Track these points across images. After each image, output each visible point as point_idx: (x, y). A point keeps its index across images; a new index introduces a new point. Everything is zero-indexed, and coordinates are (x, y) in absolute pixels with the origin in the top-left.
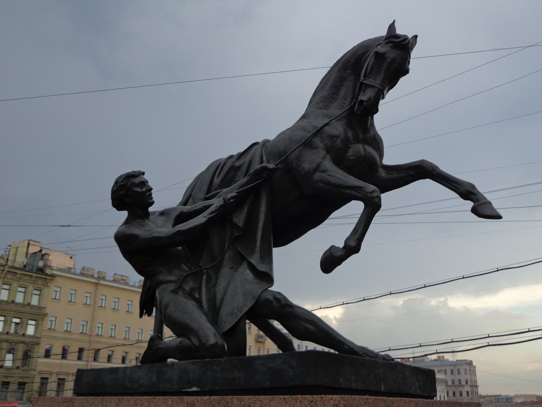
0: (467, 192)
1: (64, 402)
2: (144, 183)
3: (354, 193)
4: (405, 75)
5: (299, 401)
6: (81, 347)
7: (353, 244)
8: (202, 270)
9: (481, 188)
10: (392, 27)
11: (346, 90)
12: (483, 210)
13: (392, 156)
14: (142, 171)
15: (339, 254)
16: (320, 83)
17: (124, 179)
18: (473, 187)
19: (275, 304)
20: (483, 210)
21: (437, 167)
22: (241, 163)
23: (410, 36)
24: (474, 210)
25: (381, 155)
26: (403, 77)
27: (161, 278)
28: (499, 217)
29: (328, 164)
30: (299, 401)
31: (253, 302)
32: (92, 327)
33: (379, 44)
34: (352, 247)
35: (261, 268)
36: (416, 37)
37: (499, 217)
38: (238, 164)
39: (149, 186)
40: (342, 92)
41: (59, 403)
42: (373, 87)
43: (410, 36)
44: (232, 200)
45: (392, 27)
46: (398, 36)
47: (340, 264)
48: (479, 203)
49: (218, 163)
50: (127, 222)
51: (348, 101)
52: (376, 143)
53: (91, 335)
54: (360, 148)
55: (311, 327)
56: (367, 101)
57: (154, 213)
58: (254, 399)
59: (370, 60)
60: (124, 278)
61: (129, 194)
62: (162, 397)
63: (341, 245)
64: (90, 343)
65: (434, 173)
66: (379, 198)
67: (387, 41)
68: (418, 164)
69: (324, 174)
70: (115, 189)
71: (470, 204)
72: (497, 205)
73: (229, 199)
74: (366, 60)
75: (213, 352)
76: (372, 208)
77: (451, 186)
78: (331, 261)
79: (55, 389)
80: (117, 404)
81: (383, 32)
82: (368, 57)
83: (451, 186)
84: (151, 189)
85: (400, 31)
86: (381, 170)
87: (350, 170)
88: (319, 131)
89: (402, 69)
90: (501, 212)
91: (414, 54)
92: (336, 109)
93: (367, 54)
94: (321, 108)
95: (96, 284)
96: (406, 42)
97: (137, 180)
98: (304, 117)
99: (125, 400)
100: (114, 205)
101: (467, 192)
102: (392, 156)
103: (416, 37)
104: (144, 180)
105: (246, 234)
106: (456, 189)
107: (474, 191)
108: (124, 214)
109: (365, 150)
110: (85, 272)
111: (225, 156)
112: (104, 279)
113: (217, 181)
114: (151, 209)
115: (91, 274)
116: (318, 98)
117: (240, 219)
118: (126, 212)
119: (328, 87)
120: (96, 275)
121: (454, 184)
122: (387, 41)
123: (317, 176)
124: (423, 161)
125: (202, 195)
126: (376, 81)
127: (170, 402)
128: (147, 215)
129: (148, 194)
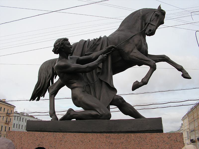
0: (180, 69)
3: (145, 62)
5: (164, 135)
7: (145, 81)
10: (160, 7)
12: (186, 76)
19: (120, 100)
20: (186, 76)
22: (99, 43)
24: (182, 75)
29: (136, 50)
30: (164, 135)
31: (112, 99)
34: (145, 82)
38: (98, 43)
44: (106, 57)
45: (160, 7)
56: (153, 30)
58: (91, 137)
61: (64, 47)
65: (169, 60)
71: (181, 73)
76: (153, 68)
77: (174, 66)
78: (136, 86)
83: (175, 66)
84: (62, 47)
98: (118, 30)
99: (68, 134)
101: (180, 69)
103: (33, 98)
104: (92, 42)
105: (103, 72)
106: (176, 67)
118: (59, 54)
122: (159, 11)
123: (132, 54)
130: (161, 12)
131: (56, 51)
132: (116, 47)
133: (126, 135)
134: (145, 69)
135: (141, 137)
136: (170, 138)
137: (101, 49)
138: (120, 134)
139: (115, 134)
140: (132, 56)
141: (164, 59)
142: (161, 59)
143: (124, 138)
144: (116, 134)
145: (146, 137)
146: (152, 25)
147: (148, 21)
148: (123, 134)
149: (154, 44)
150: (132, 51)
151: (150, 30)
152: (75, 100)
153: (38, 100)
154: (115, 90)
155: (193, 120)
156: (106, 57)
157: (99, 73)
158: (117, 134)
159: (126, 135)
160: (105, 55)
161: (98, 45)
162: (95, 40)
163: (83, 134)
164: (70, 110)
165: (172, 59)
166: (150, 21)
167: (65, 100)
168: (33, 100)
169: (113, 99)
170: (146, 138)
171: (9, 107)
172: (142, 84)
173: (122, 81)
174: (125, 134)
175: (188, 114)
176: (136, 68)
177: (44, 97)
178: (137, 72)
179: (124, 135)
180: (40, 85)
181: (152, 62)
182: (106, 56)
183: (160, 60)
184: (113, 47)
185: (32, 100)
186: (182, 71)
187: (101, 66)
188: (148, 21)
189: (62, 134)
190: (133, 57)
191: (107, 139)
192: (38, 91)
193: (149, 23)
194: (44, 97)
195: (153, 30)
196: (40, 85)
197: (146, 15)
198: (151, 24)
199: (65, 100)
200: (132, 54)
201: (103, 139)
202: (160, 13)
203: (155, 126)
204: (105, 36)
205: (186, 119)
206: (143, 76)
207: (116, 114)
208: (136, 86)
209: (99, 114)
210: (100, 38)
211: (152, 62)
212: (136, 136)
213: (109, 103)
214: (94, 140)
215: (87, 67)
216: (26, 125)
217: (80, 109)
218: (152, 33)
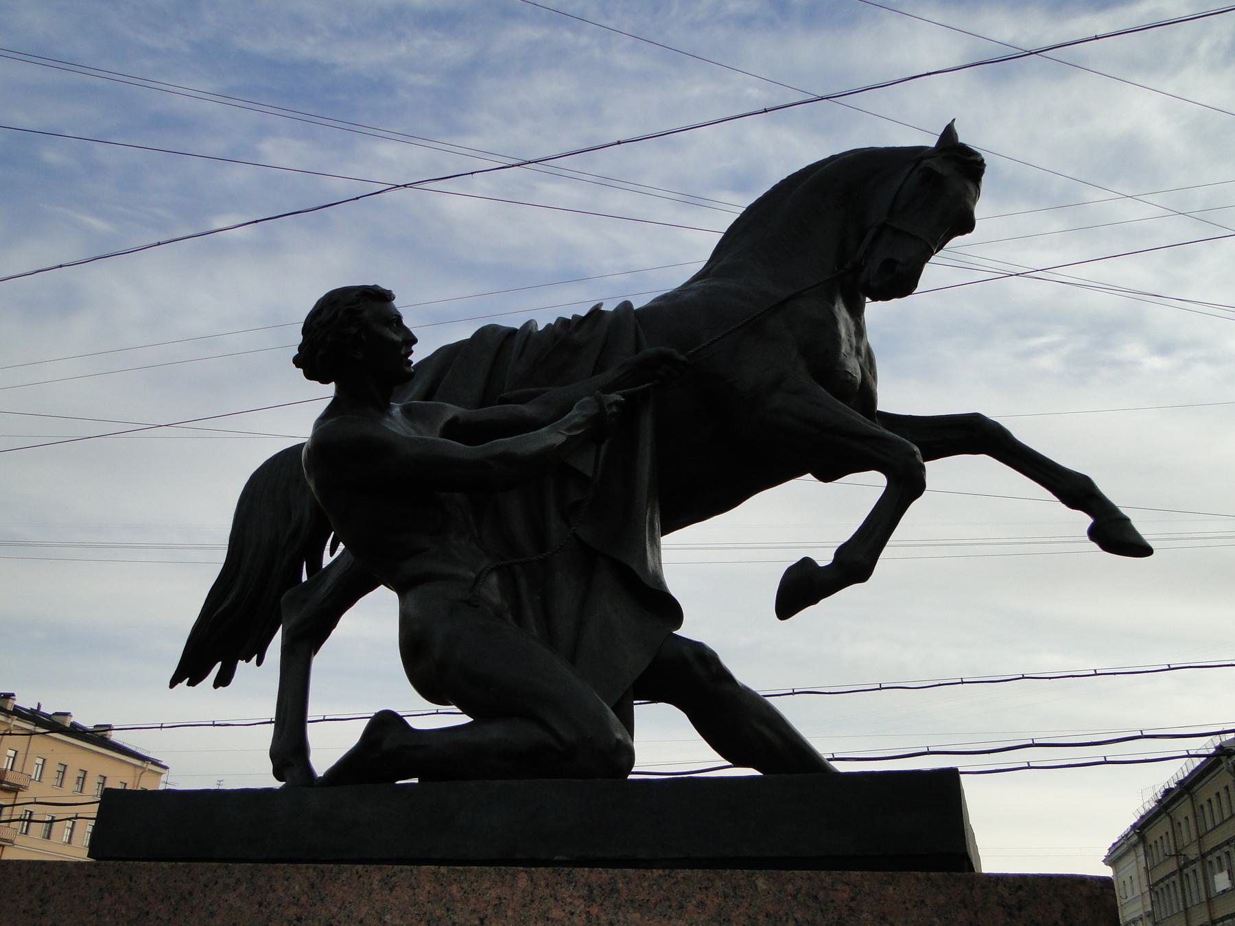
0: (1074, 490)
12: (1115, 535)
13: (897, 395)
20: (1115, 535)
24: (1095, 534)
34: (857, 560)
39: (407, 331)
72: (1144, 527)
76: (905, 488)
78: (801, 588)
84: (415, 341)
85: (962, 138)
99: (344, 876)
101: (1074, 490)
102: (897, 395)
103: (190, 669)
118: (332, 385)
131: (314, 358)
132: (683, 358)
133: (718, 883)
134: (865, 489)
135: (821, 895)
136: (1020, 909)
138: (681, 873)
139: (648, 874)
141: (975, 435)
143: (708, 902)
144: (657, 872)
145: (853, 899)
147: (889, 210)
148: (699, 872)
149: (919, 349)
151: (889, 265)
152: (425, 664)
153: (223, 680)
154: (672, 612)
155: (1172, 866)
156: (614, 409)
158: (661, 872)
159: (718, 883)
160: (616, 397)
162: (563, 322)
163: (443, 869)
164: (385, 725)
165: (1023, 434)
167: (364, 669)
168: (192, 683)
170: (852, 904)
171: (131, 769)
173: (718, 570)
174: (710, 873)
175: (1142, 827)
176: (803, 488)
177: (259, 663)
178: (809, 513)
179: (705, 884)
181: (905, 453)
185: (189, 684)
187: (586, 464)
189: (310, 871)
191: (595, 910)
194: (259, 663)
199: (364, 669)
201: (568, 908)
203: (921, 811)
204: (627, 305)
205: (1131, 858)
206: (847, 527)
207: (665, 743)
208: (801, 588)
210: (596, 312)
211: (905, 453)
212: (790, 888)
214: (510, 913)
217: (451, 718)
218: (900, 283)
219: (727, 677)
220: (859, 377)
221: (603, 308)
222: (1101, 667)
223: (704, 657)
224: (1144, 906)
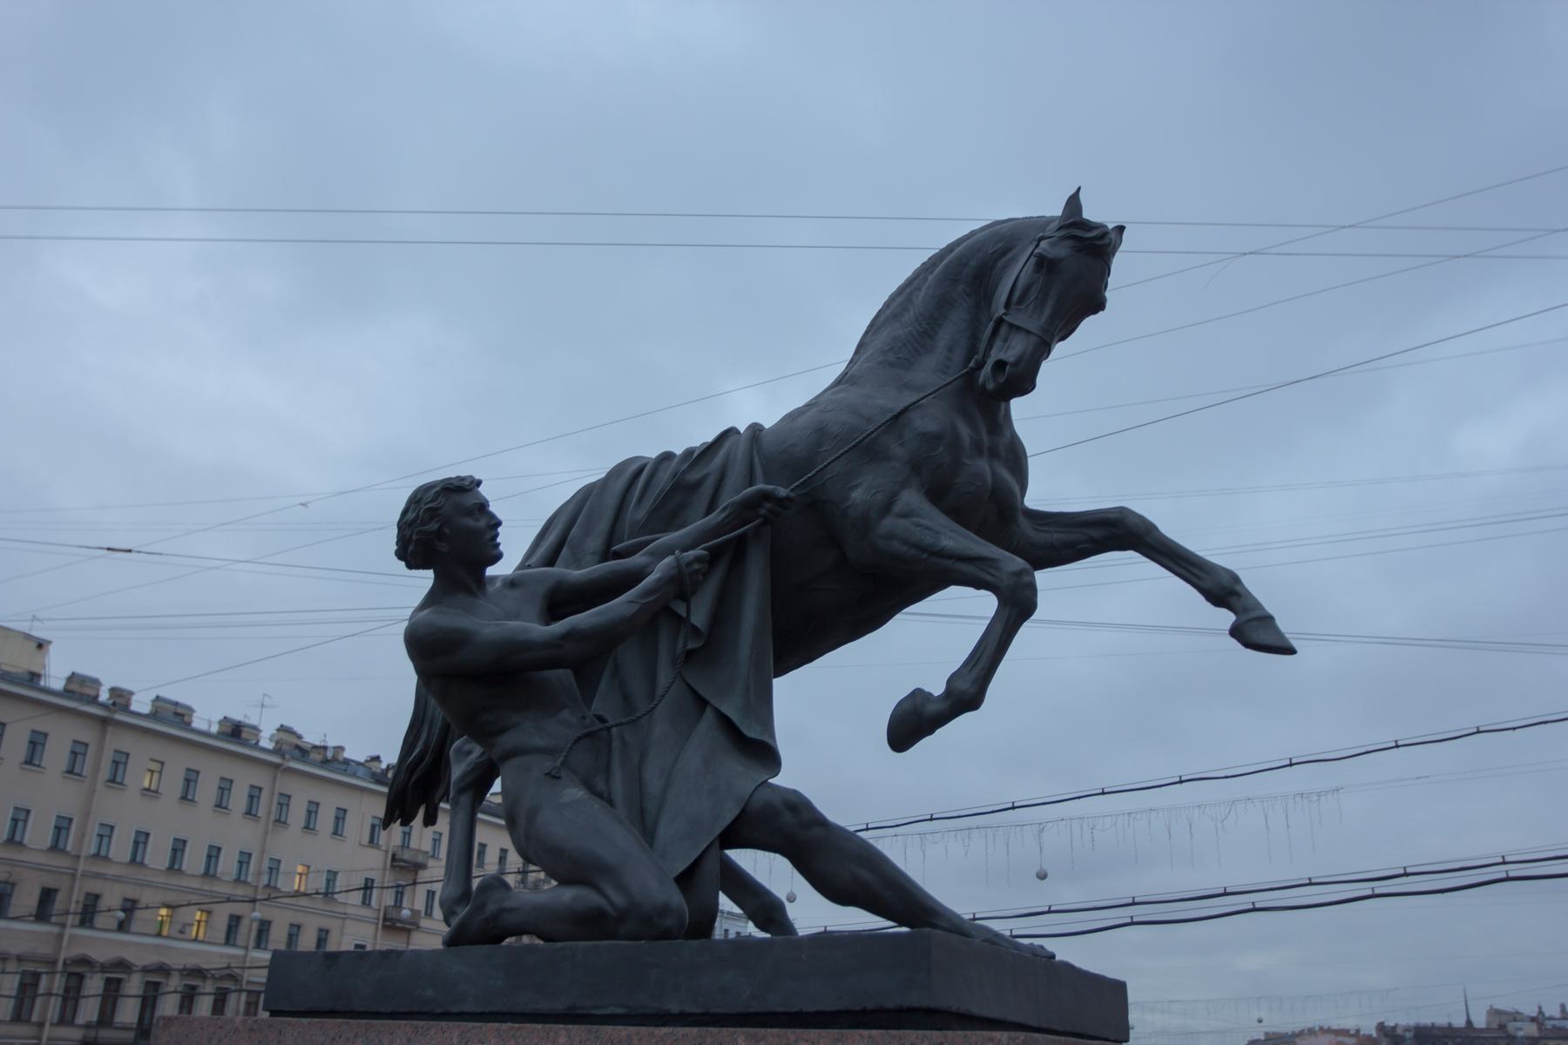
0: (1220, 588)
1: (251, 1030)
2: (483, 507)
4: (1095, 312)
6: (48, 885)
7: (964, 686)
8: (608, 729)
9: (1253, 583)
10: (1074, 203)
11: (951, 330)
12: (1258, 633)
13: (1049, 489)
14: (477, 477)
15: (932, 708)
16: (887, 305)
17: (438, 494)
18: (1236, 579)
19: (788, 818)
20: (1258, 633)
21: (1155, 528)
23: (1111, 226)
24: (1236, 632)
25: (1024, 487)
26: (1092, 317)
27: (507, 740)
28: (1290, 651)
29: (912, 498)
31: (737, 812)
32: (84, 835)
33: (1042, 238)
34: (966, 694)
35: (752, 732)
36: (1121, 229)
37: (1290, 651)
38: (694, 476)
39: (492, 516)
40: (945, 336)
41: (236, 1030)
42: (1029, 332)
43: (1111, 226)
44: (696, 566)
45: (1074, 203)
46: (1087, 226)
47: (930, 731)
48: (1252, 615)
49: (634, 467)
50: (431, 599)
51: (959, 355)
52: (1016, 460)
53: (78, 857)
54: (983, 465)
55: (865, 875)
56: (1015, 364)
57: (494, 578)
59: (1018, 270)
60: (179, 710)
61: (447, 531)
62: (539, 1026)
63: (937, 688)
64: (73, 876)
66: (1032, 588)
67: (1063, 233)
68: (1112, 516)
69: (903, 522)
70: (411, 516)
71: (1227, 618)
72: (1286, 625)
73: (689, 564)
74: (1006, 267)
75: (648, 926)
76: (1017, 607)
78: (912, 724)
79: (14, 993)
80: (409, 1040)
81: (1055, 209)
82: (1014, 260)
84: (499, 524)
85: (1090, 213)
86: (1022, 520)
87: (958, 515)
88: (898, 418)
89: (1087, 299)
90: (1295, 644)
91: (1119, 263)
92: (930, 372)
93: (1009, 255)
94: (892, 365)
95: (104, 722)
96: (1105, 241)
97: (468, 500)
98: (839, 382)
99: (432, 1032)
100: (402, 554)
101: (1220, 588)
102: (1049, 489)
103: (1121, 229)
105: (708, 650)
107: (1238, 588)
108: (425, 579)
109: (994, 473)
110: (74, 687)
111: (652, 453)
112: (125, 708)
113: (637, 513)
114: (491, 571)
115: (93, 693)
116: (885, 335)
117: (699, 615)
118: (430, 574)
119: (909, 316)
120: (104, 696)
121: (1196, 571)
122: (1063, 233)
124: (1122, 511)
125: (595, 543)
126: (1029, 319)
127: (562, 1040)
128: (480, 581)
129: (488, 536)
130: (1074, 237)
137: (708, 513)
140: (889, 537)
141: (1115, 532)
142: (1096, 533)
146: (1018, 328)
147: (1024, 288)
149: (1070, 434)
150: (886, 508)
154: (766, 755)
157: (690, 654)
161: (697, 485)
166: (1008, 305)
169: (743, 811)
172: (942, 706)
178: (934, 633)
180: (424, 736)
182: (698, 559)
183: (1092, 540)
184: (765, 496)
186: (1234, 600)
188: (1024, 288)
190: (896, 546)
192: (412, 772)
193: (1000, 321)
195: (1020, 359)
196: (424, 736)
197: (1000, 263)
198: (1011, 326)
200: (888, 523)
202: (1070, 243)
208: (912, 724)
209: (609, 909)
213: (718, 831)
215: (570, 635)
216: (788, 906)
219: (822, 822)
220: (989, 478)
221: (347, 755)
222: (1403, 737)
223: (797, 805)
224: (1551, 1018)
